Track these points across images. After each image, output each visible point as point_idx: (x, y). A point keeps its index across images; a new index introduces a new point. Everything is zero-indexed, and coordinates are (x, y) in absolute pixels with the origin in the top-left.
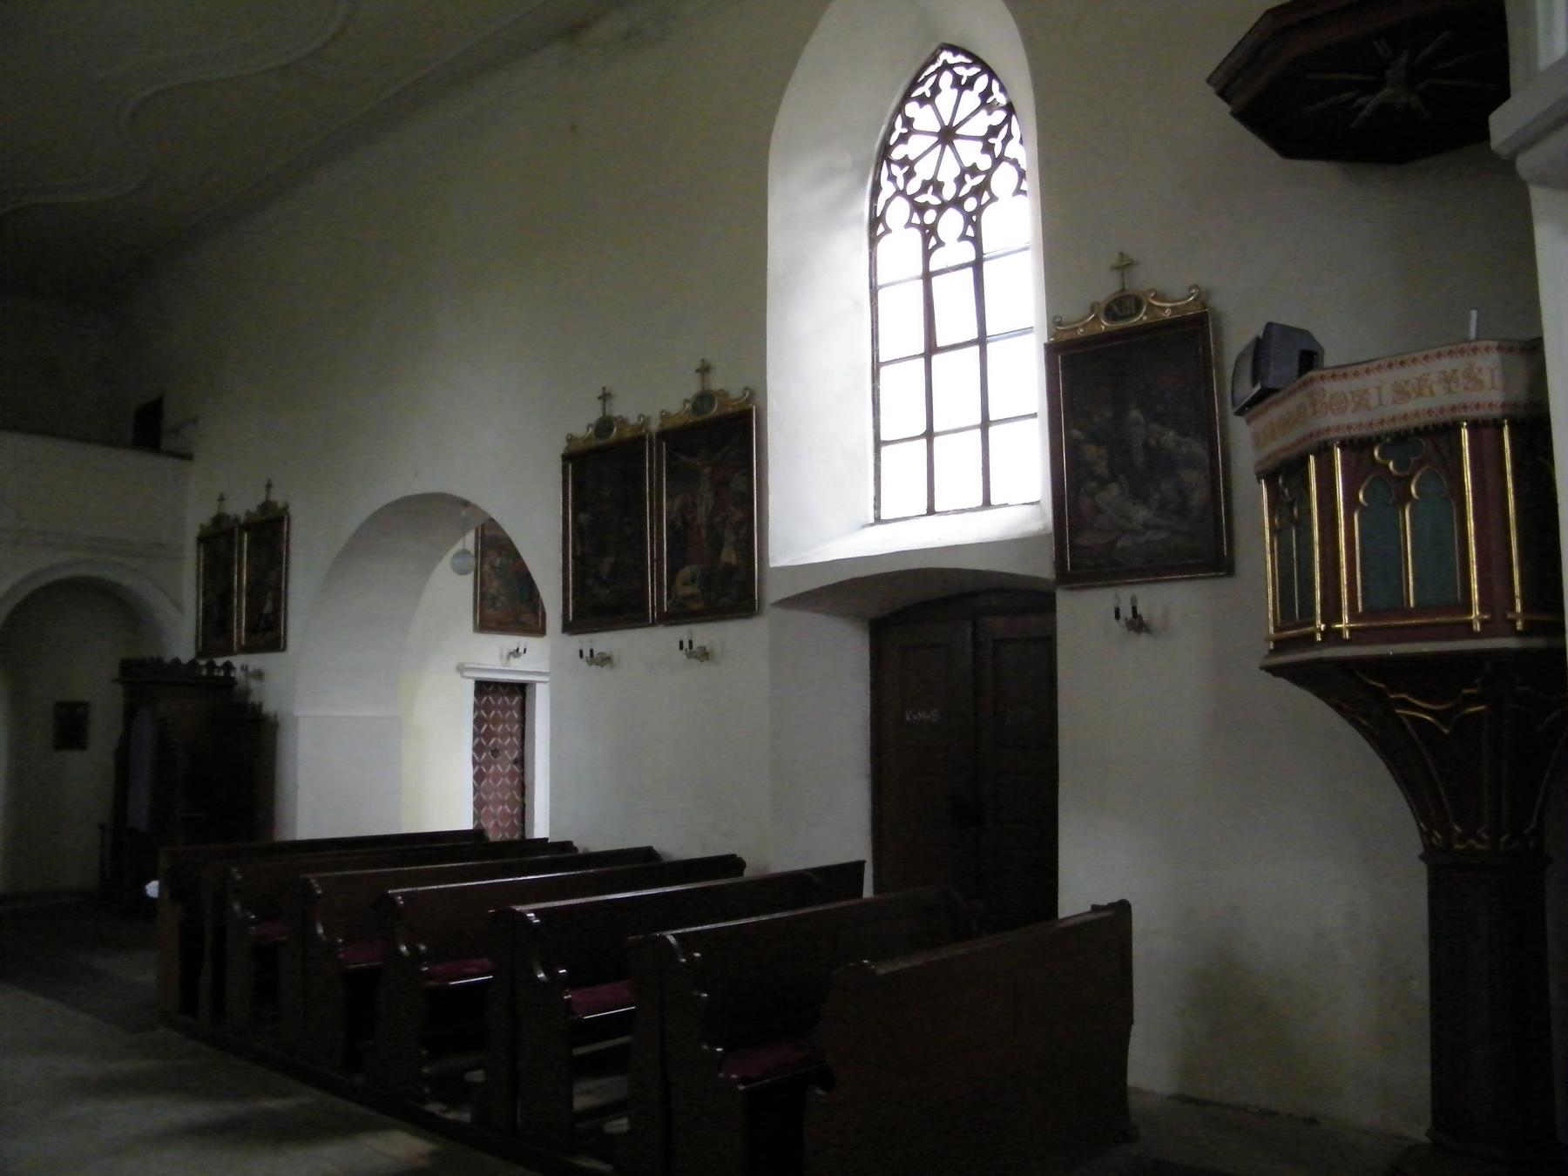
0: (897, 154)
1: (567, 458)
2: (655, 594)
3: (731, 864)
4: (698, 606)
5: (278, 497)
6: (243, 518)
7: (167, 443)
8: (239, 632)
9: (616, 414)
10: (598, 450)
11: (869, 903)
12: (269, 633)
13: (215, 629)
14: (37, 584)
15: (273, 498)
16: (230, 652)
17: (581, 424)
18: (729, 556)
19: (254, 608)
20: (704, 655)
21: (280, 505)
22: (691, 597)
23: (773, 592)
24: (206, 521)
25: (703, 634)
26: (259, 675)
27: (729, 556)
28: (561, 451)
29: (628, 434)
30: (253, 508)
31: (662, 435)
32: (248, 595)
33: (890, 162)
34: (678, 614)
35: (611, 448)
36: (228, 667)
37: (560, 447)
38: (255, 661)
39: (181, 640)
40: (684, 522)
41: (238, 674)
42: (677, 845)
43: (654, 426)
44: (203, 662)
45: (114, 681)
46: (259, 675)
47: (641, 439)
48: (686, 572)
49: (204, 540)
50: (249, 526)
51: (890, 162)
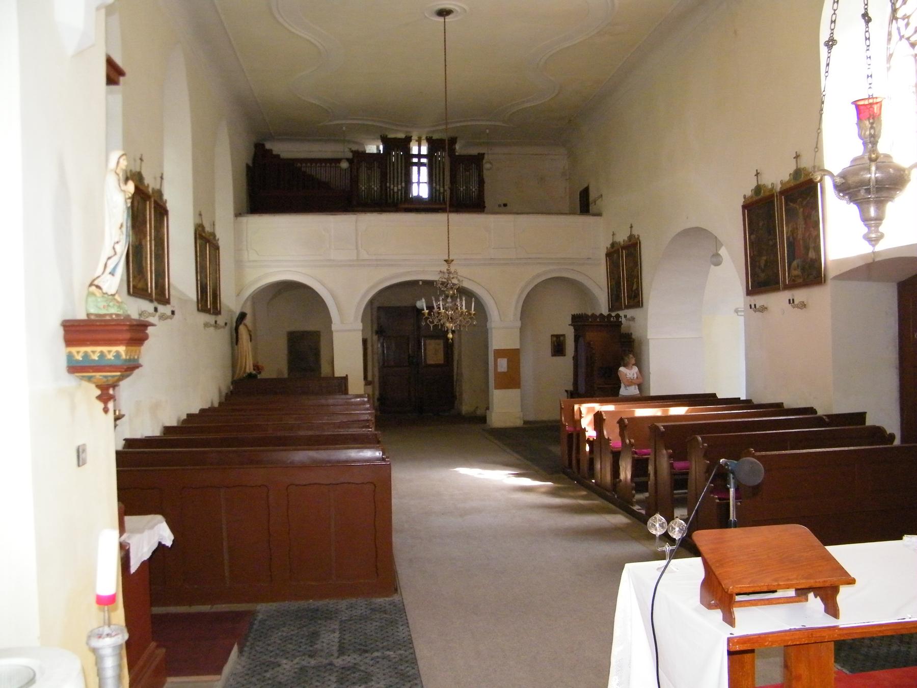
0: (899, 14)
1: (744, 207)
2: (784, 275)
3: (811, 410)
4: (800, 280)
5: (635, 233)
6: (622, 243)
7: (592, 208)
8: (625, 300)
9: (802, 166)
10: (757, 202)
11: (897, 448)
12: (636, 299)
13: (615, 301)
14: (524, 296)
15: (633, 233)
16: (620, 309)
17: (748, 189)
18: (812, 254)
19: (630, 286)
20: (803, 305)
21: (770, 187)
22: (798, 276)
23: (832, 273)
24: (749, 193)
25: (800, 295)
26: (633, 319)
27: (812, 254)
28: (742, 204)
29: (768, 194)
30: (786, 177)
31: (782, 193)
32: (627, 281)
33: (896, 19)
34: (793, 285)
35: (761, 200)
36: (618, 316)
37: (741, 201)
38: (630, 313)
39: (603, 308)
40: (794, 238)
41: (623, 320)
42: (790, 402)
43: (778, 188)
44: (613, 314)
45: (566, 391)
46: (633, 319)
47: (772, 196)
48: (795, 263)
49: (609, 255)
50: (623, 248)
51: (896, 19)
